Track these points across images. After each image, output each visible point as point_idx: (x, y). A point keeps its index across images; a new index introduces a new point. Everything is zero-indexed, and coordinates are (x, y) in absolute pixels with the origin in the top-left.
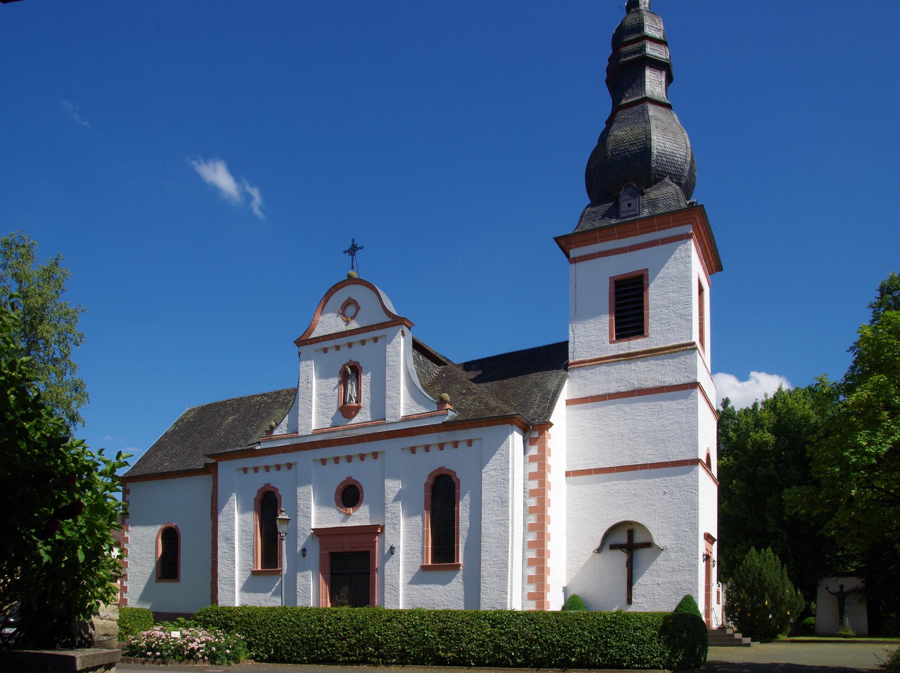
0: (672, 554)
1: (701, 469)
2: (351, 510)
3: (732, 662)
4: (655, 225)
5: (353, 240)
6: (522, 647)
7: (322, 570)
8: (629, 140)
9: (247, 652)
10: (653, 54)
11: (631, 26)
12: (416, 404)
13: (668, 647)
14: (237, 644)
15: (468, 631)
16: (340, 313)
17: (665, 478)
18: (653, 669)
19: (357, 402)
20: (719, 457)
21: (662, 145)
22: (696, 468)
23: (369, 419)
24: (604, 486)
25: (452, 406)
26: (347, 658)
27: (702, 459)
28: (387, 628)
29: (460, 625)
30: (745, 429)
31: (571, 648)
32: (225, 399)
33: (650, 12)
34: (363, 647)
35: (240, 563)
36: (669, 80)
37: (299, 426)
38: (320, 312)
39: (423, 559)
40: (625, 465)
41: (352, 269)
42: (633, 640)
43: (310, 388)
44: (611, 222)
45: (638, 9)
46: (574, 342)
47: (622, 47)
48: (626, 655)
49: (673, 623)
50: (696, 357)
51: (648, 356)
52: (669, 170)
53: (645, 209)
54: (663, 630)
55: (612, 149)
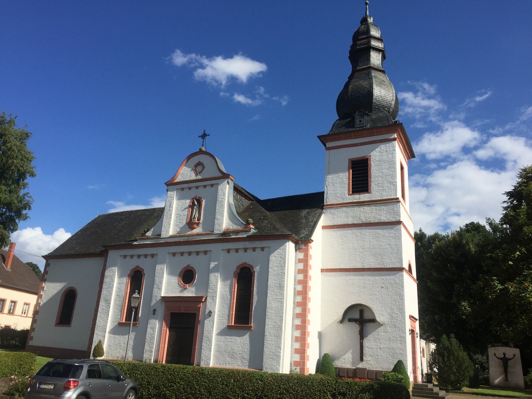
0: (389, 328)
5: (204, 131)
7: (165, 319)
12: (232, 224)
21: (379, 91)
36: (384, 57)
40: (357, 268)
43: (171, 210)
47: (358, 41)
50: (399, 207)
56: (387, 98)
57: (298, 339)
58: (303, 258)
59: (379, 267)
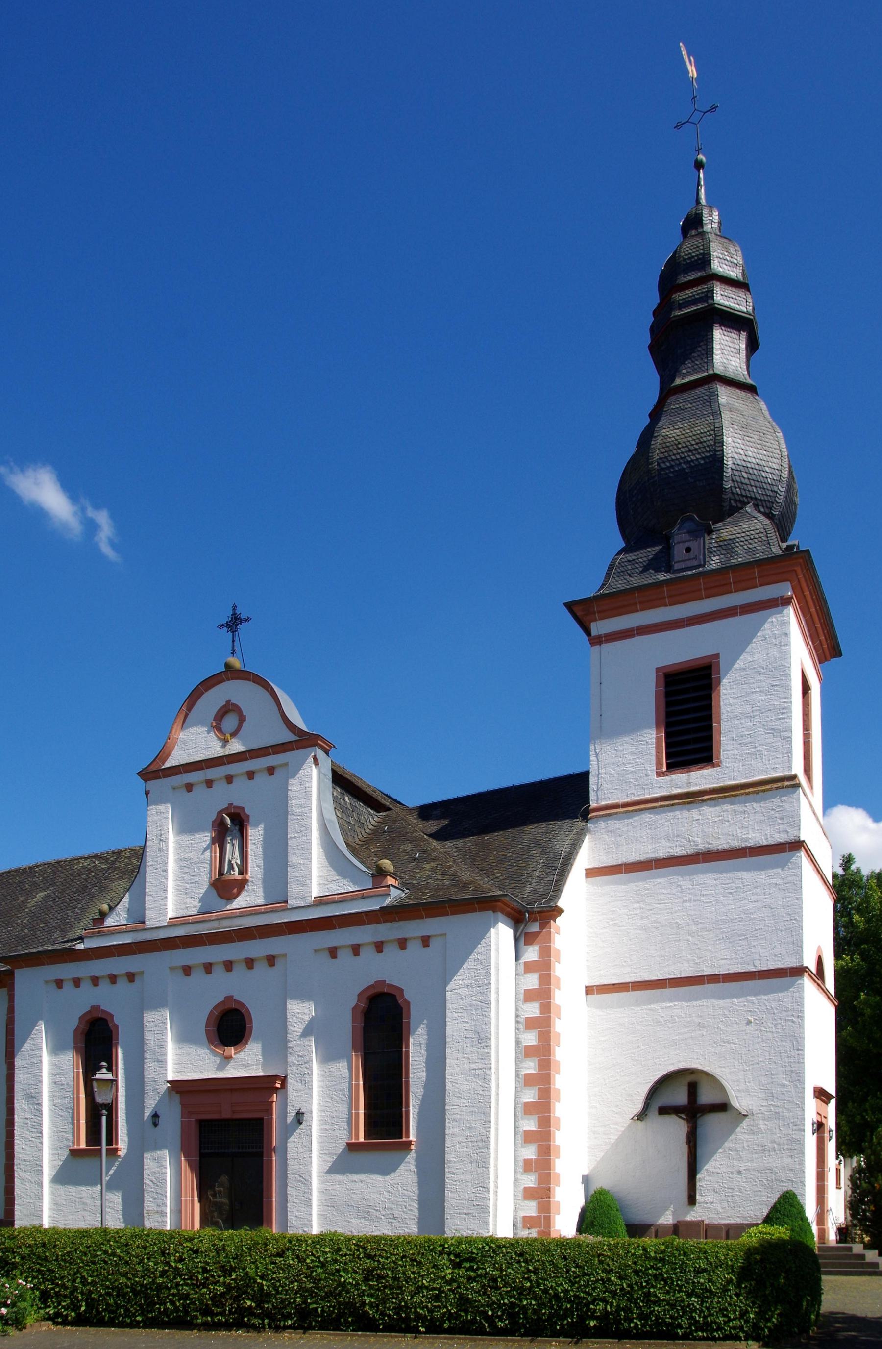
0: (761, 1122)
1: (807, 984)
2: (232, 1050)
3: (864, 1315)
4: (731, 583)
5: (235, 608)
6: (506, 1301)
7: (185, 1149)
8: (688, 443)
9: (41, 1308)
10: (726, 303)
11: (689, 258)
12: (337, 878)
13: (754, 1303)
14: (20, 1296)
15: (413, 1273)
16: (214, 727)
17: (749, 998)
18: (729, 1340)
19: (241, 873)
20: (837, 955)
21: (741, 452)
22: (799, 982)
23: (261, 901)
24: (650, 1010)
25: (396, 879)
26: (209, 1319)
27: (809, 967)
28: (277, 1267)
29: (400, 1263)
30: (878, 909)
31: (589, 1303)
32: (32, 863)
33: (721, 236)
34: (236, 1299)
35: (51, 1137)
36: (753, 345)
37: (146, 912)
38: (181, 725)
39: (350, 1132)
40: (683, 976)
41: (233, 654)
42: (693, 1290)
43: (165, 849)
44: (658, 577)
45: (700, 230)
46: (599, 774)
47: (676, 292)
48: (681, 1317)
49: (762, 1260)
50: (799, 799)
51: (719, 798)
52: (752, 493)
53: (714, 556)
54: (744, 1274)
55: (660, 459)
56: (763, 474)
57: (532, 1165)
58: (536, 959)
59: (740, 971)
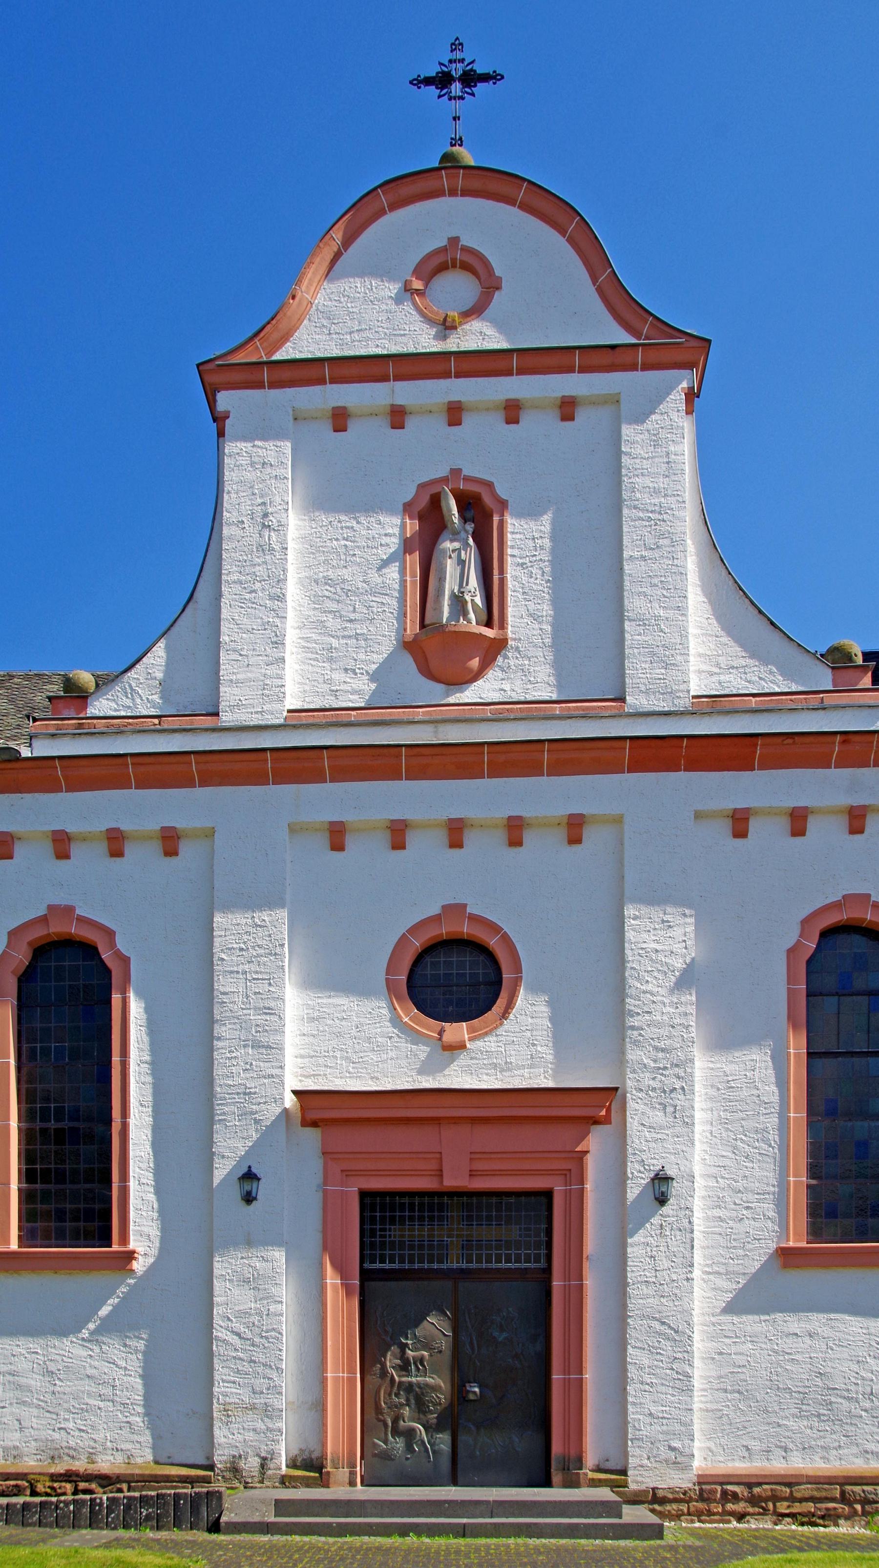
5: (250, 1167)
43: (277, 547)
